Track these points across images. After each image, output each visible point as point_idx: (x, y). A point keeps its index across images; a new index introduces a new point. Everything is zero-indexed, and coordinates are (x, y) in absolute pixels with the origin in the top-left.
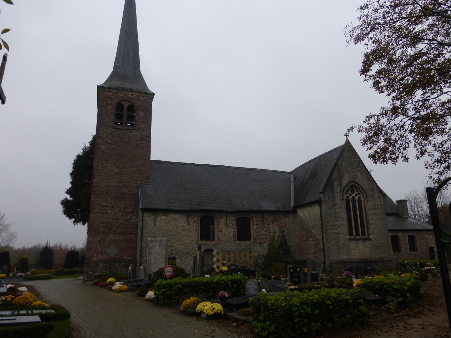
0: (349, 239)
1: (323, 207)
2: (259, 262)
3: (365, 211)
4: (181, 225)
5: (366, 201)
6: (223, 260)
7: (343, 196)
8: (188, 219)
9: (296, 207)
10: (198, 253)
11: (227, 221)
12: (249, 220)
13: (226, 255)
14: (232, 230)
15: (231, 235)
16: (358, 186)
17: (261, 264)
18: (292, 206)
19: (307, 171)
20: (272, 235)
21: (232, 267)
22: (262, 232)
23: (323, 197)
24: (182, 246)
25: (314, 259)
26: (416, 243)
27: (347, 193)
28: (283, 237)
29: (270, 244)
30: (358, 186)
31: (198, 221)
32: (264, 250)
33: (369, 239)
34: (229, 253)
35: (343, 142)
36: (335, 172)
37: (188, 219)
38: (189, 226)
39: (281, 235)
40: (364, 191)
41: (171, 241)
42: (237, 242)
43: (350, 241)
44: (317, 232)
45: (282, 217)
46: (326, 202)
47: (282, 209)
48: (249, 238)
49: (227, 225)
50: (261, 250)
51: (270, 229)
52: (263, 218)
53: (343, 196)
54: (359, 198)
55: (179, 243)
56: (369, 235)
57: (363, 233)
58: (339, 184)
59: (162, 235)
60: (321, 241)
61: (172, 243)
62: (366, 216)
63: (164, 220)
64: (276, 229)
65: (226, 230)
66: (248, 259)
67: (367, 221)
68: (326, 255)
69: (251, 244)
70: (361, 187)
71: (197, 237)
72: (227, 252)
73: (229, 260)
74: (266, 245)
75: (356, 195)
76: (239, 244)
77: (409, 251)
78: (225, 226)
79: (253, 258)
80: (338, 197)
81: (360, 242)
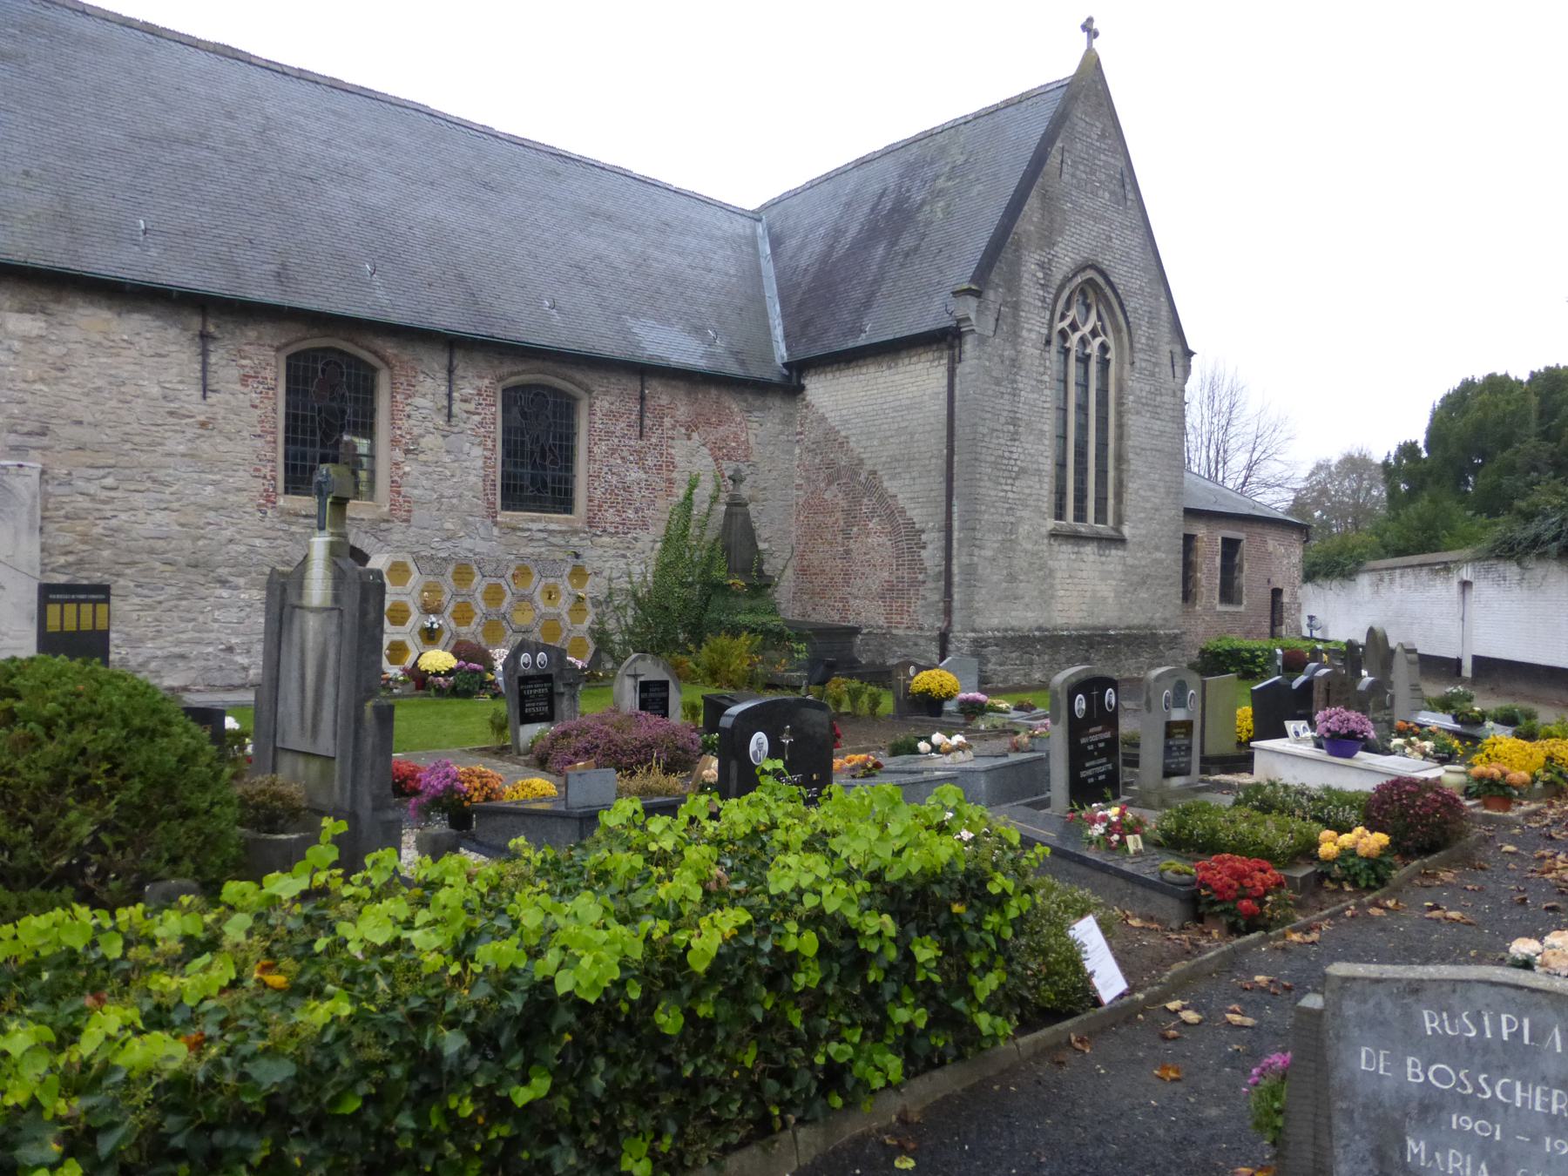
0: (1055, 535)
1: (961, 369)
2: (611, 625)
3: (1120, 415)
4: (155, 390)
5: (1127, 366)
6: (427, 610)
7: (1050, 327)
8: (205, 354)
9: (799, 368)
10: (320, 544)
11: (450, 396)
12: (565, 408)
13: (448, 585)
14: (477, 451)
15: (472, 479)
16: (1108, 291)
17: (617, 638)
18: (779, 362)
19: (848, 205)
20: (681, 492)
21: (525, 658)
22: (635, 474)
23: (972, 316)
24: (159, 516)
25: (882, 621)
26: (1241, 571)
27: (1063, 317)
28: (736, 506)
29: (667, 540)
30: (1108, 291)
31: (275, 375)
32: (637, 569)
33: (1119, 541)
34: (463, 573)
35: (1065, 67)
36: (1033, 202)
37: (205, 354)
38: (213, 398)
39: (724, 497)
40: (1126, 318)
41: (80, 484)
42: (505, 517)
43: (1055, 544)
44: (915, 496)
45: (735, 408)
46: (982, 340)
47: (732, 368)
48: (564, 502)
49: (450, 416)
50: (622, 563)
51: (672, 465)
52: (642, 399)
53: (1050, 327)
54: (1104, 348)
55: (138, 500)
56: (1120, 520)
57: (1101, 516)
58: (1041, 266)
59: (13, 439)
60: (933, 538)
61: (93, 498)
62: (1120, 437)
63: (26, 340)
64: (703, 464)
65: (435, 446)
66: (563, 605)
67: (1120, 459)
68: (956, 604)
69: (575, 532)
70: (1117, 295)
71: (267, 471)
72: (451, 568)
73: (463, 614)
74: (648, 544)
75: (1094, 333)
76: (514, 529)
77: (1217, 601)
78: (441, 422)
79: (588, 605)
80: (1034, 326)
81: (1089, 550)
